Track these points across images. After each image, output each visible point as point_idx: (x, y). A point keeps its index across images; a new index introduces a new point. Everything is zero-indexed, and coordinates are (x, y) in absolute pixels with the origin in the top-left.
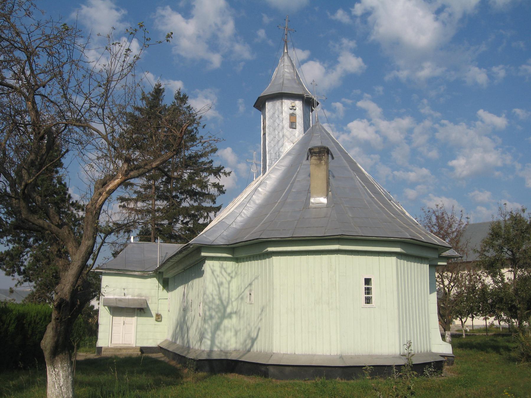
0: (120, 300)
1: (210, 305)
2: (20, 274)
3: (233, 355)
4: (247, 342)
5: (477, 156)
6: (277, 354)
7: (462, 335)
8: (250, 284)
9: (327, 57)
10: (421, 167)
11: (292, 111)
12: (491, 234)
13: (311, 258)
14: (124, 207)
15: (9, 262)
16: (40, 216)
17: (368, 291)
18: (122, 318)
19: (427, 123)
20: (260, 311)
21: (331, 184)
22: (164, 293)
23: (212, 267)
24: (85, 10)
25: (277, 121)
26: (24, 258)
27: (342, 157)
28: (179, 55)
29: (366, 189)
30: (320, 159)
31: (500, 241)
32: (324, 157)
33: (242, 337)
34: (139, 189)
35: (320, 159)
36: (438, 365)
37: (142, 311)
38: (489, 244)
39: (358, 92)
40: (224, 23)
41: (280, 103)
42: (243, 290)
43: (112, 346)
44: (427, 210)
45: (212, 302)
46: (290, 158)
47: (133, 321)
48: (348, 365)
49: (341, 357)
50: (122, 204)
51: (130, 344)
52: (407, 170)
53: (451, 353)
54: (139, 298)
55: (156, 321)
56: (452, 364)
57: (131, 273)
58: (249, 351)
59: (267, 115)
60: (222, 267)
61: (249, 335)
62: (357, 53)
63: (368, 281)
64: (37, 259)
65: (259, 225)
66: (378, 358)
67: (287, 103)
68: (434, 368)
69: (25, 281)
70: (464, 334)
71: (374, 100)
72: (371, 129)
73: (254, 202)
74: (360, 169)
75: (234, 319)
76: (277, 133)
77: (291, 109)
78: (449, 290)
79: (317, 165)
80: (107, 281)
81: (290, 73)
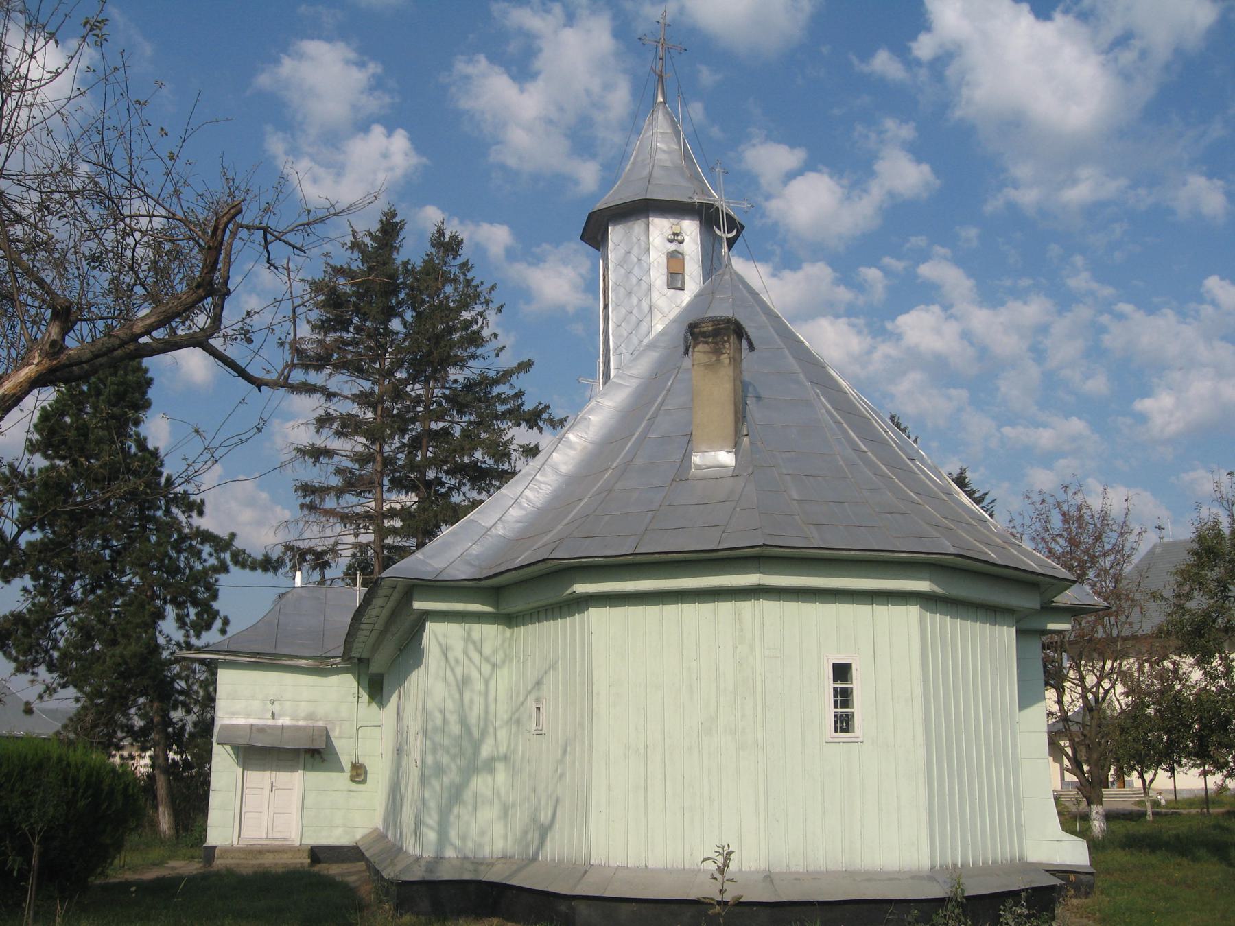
0: (262, 729)
1: (437, 738)
2: (51, 668)
3: (495, 869)
4: (530, 836)
5: (1201, 387)
6: (600, 867)
7: (1144, 814)
8: (539, 683)
9: (844, 160)
10: (1067, 416)
11: (672, 247)
12: (1195, 553)
13: (690, 610)
14: (312, 507)
15: (17, 637)
16: (111, 533)
17: (843, 697)
18: (268, 773)
19: (1083, 312)
20: (560, 752)
21: (749, 417)
22: (368, 711)
23: (443, 641)
24: (288, 66)
25: (636, 271)
26: (59, 629)
27: (787, 352)
28: (503, 167)
29: (844, 431)
30: (718, 352)
31: (1219, 571)
32: (727, 345)
33: (520, 819)
34: (348, 464)
35: (718, 352)
36: (1045, 894)
37: (316, 756)
38: (1190, 577)
39: (919, 241)
40: (608, 87)
41: (643, 225)
42: (521, 699)
43: (243, 844)
44: (1036, 498)
45: (443, 729)
46: (654, 355)
47: (293, 781)
48: (795, 899)
49: (769, 877)
50: (308, 500)
51: (285, 839)
52: (1039, 425)
53: (1088, 863)
54: (310, 723)
55: (352, 780)
56: (1087, 894)
57: (289, 662)
58: (534, 859)
59: (611, 256)
60: (467, 639)
61: (534, 819)
62: (918, 152)
63: (842, 672)
64: (86, 633)
65: (560, 527)
66: (891, 879)
67: (660, 227)
68: (1028, 907)
69: (64, 686)
70: (1150, 812)
71: (959, 261)
72: (952, 329)
73: (556, 470)
74: (836, 382)
75: (501, 776)
76: (635, 300)
77: (671, 241)
78: (1097, 700)
79: (708, 366)
80: (229, 682)
81: (668, 152)
